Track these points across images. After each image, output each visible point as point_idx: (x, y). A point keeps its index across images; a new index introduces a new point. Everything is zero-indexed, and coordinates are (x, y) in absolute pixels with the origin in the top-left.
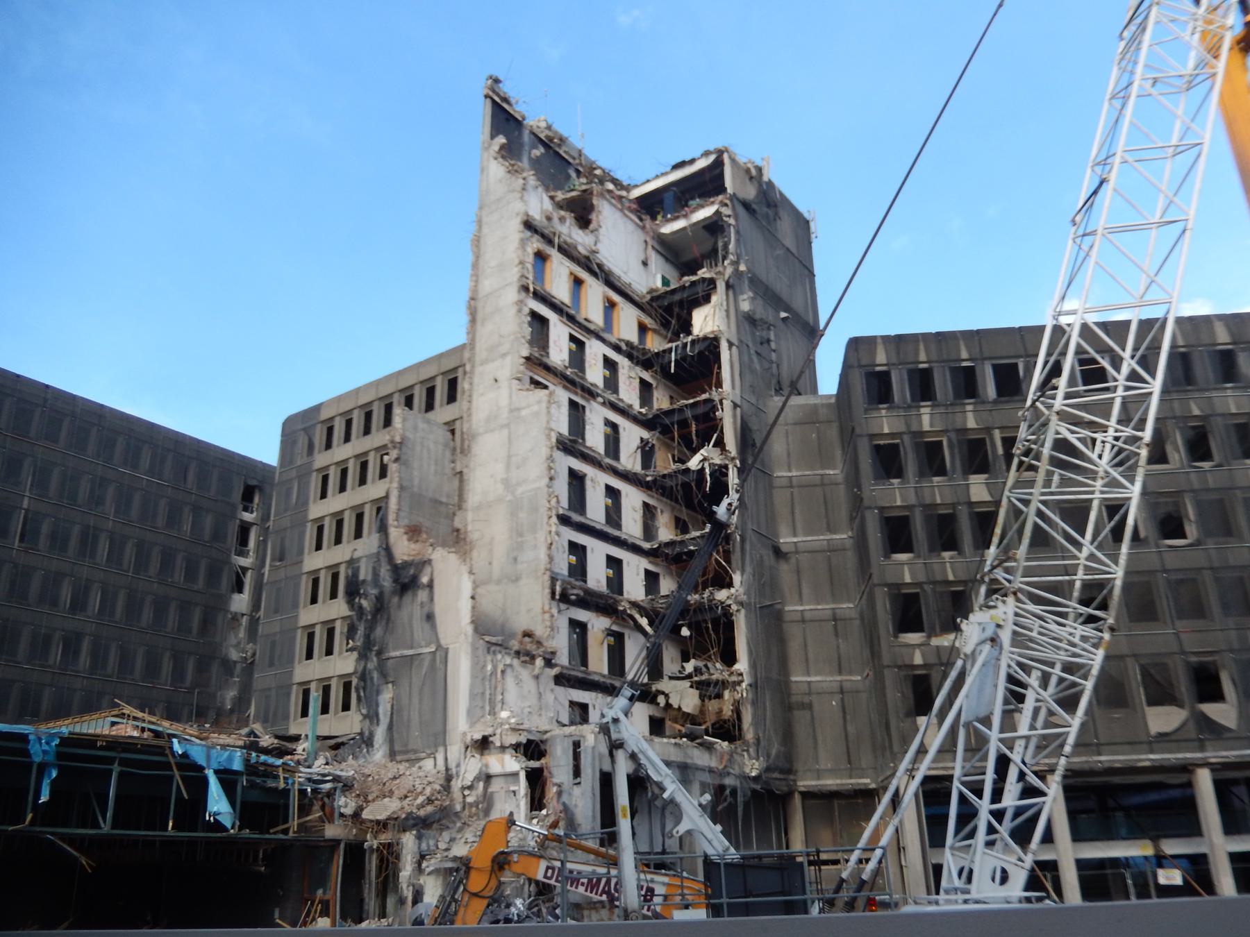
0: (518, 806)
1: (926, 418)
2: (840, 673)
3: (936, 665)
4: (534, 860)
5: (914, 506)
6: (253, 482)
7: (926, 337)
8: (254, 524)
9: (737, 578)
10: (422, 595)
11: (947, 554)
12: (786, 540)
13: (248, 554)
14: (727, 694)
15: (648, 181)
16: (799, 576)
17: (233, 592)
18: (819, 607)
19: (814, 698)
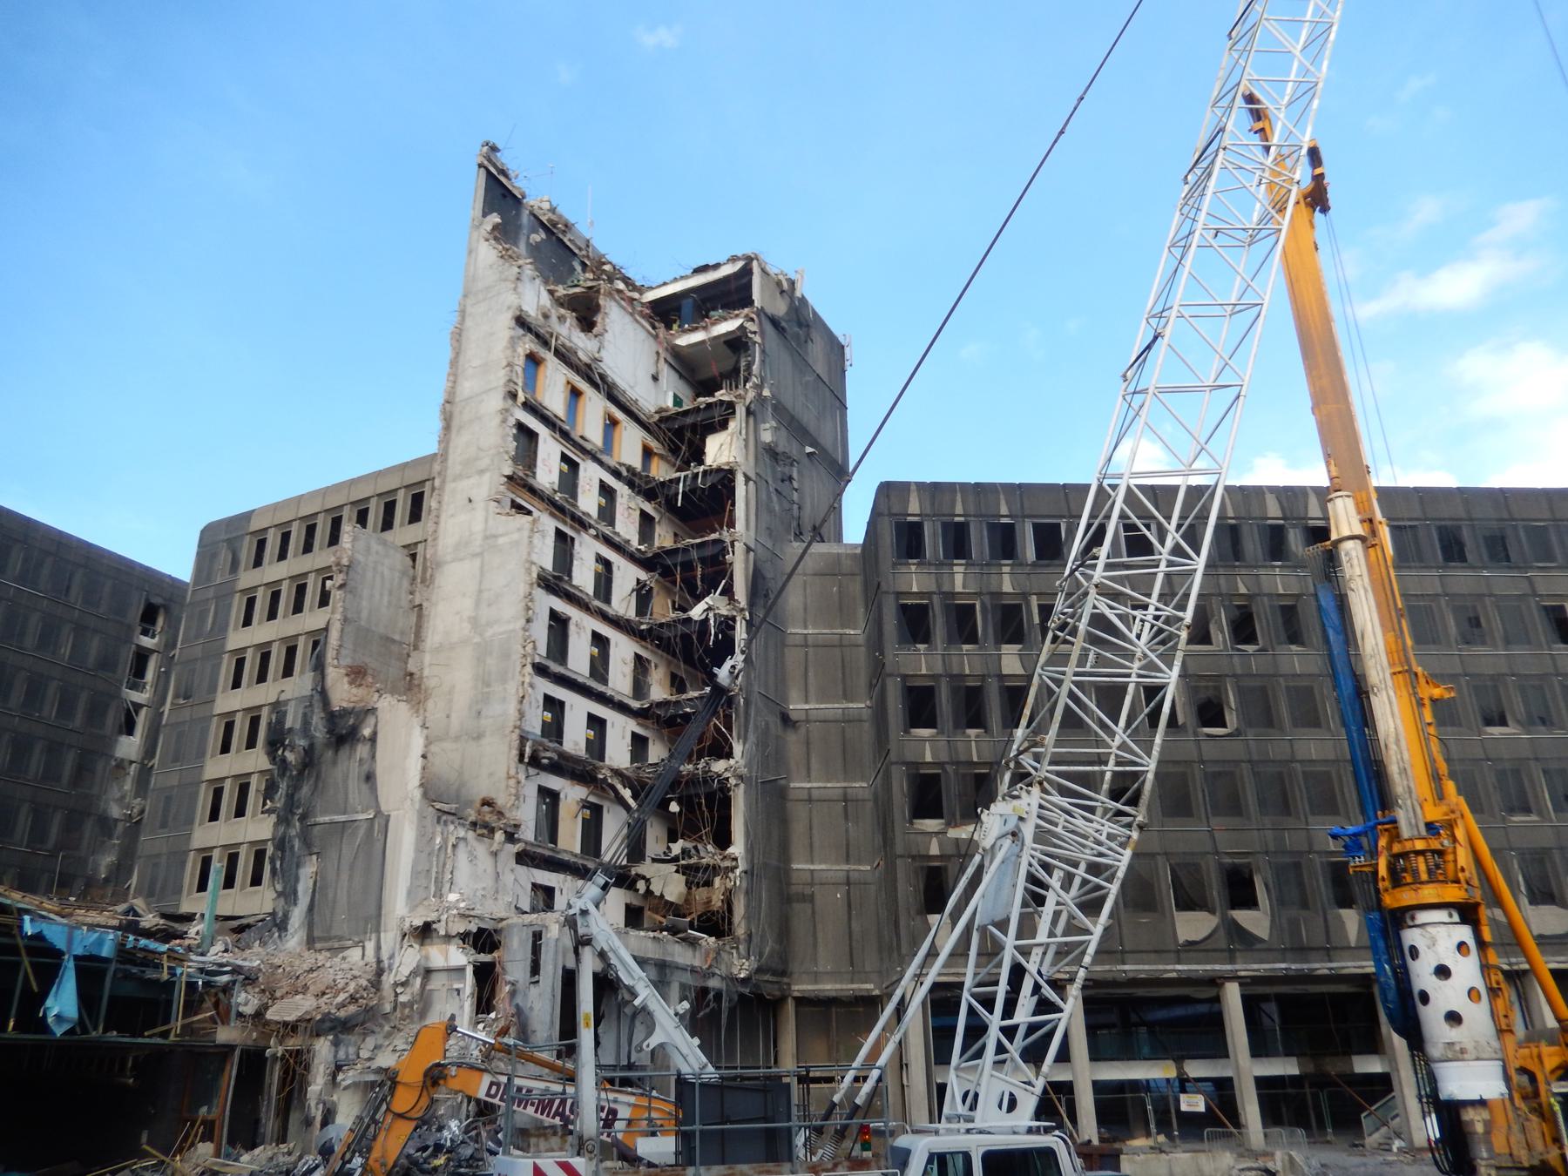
0: (462, 1007)
1: (960, 579)
2: (847, 861)
4: (477, 1074)
6: (157, 600)
7: (964, 487)
8: (154, 651)
9: (738, 749)
10: (362, 750)
11: (972, 732)
12: (796, 706)
13: (144, 687)
14: (717, 881)
15: (665, 284)
16: (808, 748)
17: (120, 733)
18: (829, 785)
19: (816, 889)
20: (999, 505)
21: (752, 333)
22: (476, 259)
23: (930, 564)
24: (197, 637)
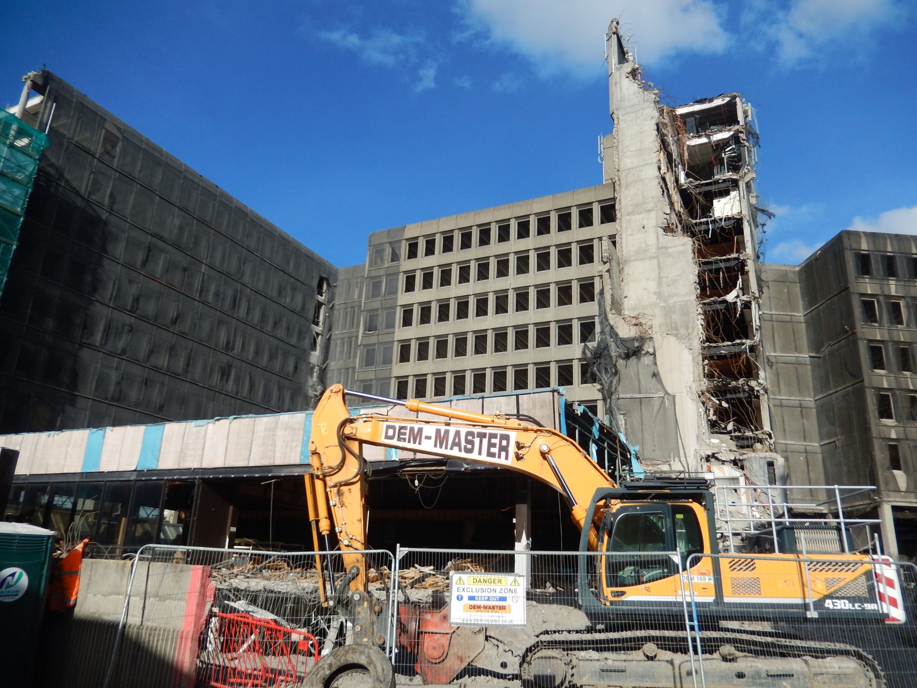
1: (893, 287)
2: (805, 440)
3: (903, 439)
5: (887, 341)
7: (890, 236)
10: (647, 360)
16: (778, 377)
18: (792, 398)
20: (911, 247)
21: (743, 139)
22: (621, 89)
23: (876, 279)
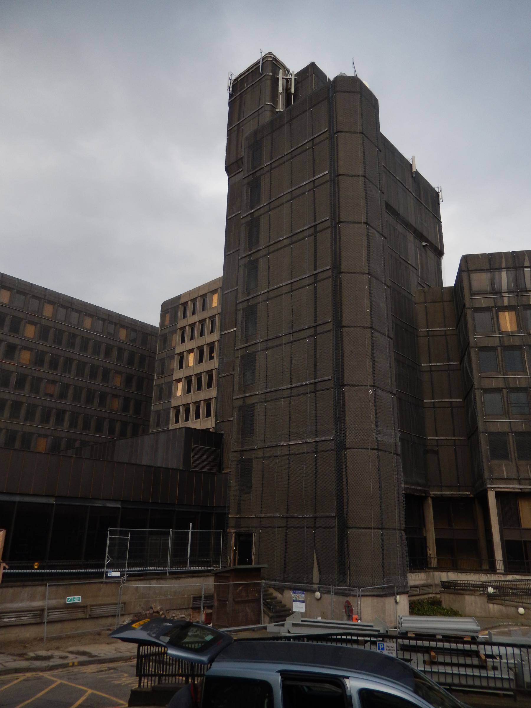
24: (164, 348)
